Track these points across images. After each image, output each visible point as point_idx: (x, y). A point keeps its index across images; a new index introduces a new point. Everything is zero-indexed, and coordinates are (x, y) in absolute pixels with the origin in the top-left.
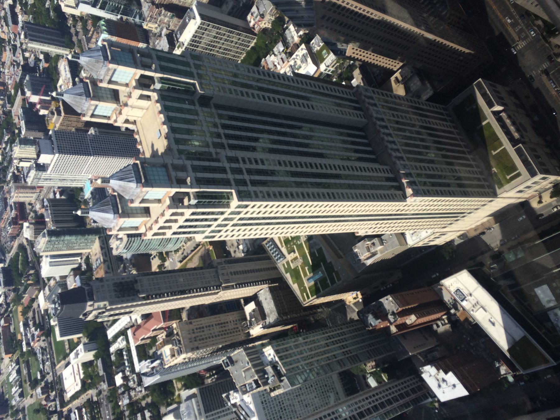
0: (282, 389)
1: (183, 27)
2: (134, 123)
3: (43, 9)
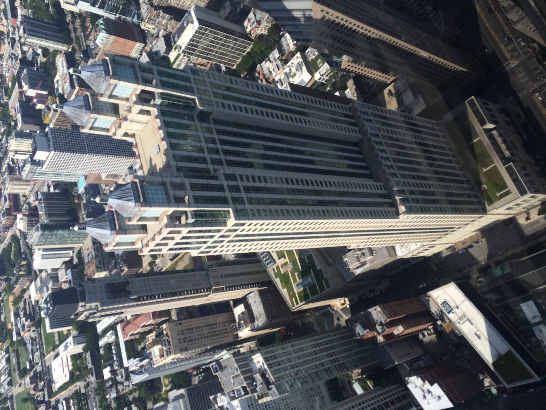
0: (270, 397)
1: (181, 30)
2: (133, 136)
3: (42, 4)
